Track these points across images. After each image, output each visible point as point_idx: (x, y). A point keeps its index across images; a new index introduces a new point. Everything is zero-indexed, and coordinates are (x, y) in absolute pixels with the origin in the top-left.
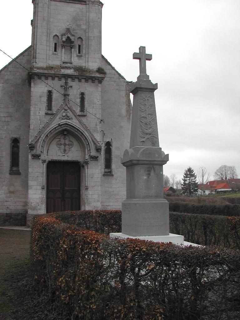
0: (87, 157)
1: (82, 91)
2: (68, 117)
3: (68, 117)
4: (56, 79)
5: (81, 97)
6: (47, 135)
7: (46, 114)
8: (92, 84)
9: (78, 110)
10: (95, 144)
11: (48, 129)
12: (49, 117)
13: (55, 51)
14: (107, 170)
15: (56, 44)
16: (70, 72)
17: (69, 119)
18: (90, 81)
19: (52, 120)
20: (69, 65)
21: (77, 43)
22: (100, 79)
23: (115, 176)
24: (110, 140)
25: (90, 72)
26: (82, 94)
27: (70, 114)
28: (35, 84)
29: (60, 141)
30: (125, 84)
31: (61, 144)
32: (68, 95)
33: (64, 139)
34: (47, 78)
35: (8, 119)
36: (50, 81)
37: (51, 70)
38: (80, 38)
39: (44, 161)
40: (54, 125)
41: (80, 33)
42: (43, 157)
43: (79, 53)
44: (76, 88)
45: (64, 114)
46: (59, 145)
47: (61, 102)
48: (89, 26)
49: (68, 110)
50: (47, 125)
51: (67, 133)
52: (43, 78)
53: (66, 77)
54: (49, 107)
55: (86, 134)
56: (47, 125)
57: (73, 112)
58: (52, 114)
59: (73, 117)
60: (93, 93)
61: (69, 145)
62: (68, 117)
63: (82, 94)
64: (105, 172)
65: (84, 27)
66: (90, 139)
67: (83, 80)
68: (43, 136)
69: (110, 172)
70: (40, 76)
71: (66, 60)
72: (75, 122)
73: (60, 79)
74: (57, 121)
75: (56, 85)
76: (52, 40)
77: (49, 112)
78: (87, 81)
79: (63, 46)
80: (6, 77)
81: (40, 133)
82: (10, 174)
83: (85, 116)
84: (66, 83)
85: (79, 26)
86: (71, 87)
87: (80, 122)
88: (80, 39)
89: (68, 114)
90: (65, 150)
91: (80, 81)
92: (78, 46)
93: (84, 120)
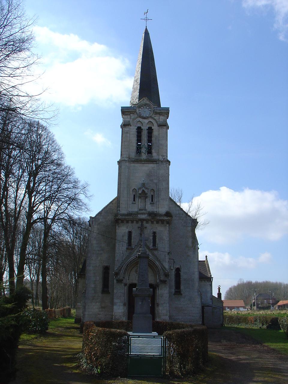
0: (158, 281)
9: (151, 246)
21: (149, 194)
28: (119, 227)
36: (130, 224)
39: (125, 285)
43: (152, 201)
53: (142, 220)
55: (157, 263)
57: (148, 248)
65: (155, 181)
68: (124, 266)
79: (140, 197)
82: (102, 293)
85: (152, 180)
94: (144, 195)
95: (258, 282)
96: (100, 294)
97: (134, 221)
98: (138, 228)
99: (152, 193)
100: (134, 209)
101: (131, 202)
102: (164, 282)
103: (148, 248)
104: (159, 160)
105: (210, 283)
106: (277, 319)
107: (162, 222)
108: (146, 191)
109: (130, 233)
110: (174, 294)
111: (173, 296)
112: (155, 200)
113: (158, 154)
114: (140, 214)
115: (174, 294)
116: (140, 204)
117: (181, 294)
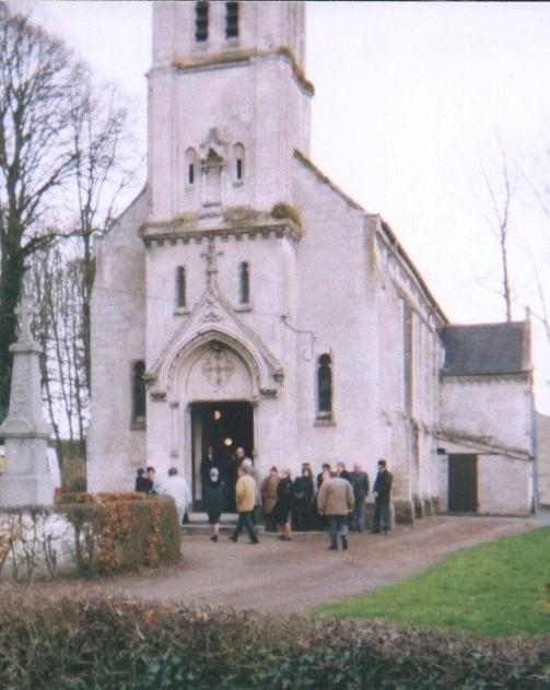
0: (256, 392)
1: (243, 260)
2: (214, 316)
3: (213, 317)
4: (180, 241)
5: (10, 343)
6: (178, 356)
7: (176, 314)
8: (265, 242)
9: (234, 299)
10: (270, 366)
11: (178, 344)
12: (182, 319)
13: (191, 181)
14: (323, 414)
15: (191, 167)
16: (214, 224)
17: (218, 320)
18: (259, 235)
19: (184, 326)
20: (214, 210)
21: (230, 157)
22: (279, 229)
23: (340, 425)
24: (328, 352)
25: (255, 217)
26: (245, 266)
27: (219, 311)
28: (152, 257)
29: (209, 363)
30: (361, 223)
31: (211, 369)
32: (215, 272)
33: (217, 358)
34: (174, 242)
35: (124, 326)
36: (180, 246)
37: (180, 225)
38: (239, 144)
39: (175, 405)
40: (190, 334)
41: (237, 135)
42: (170, 398)
43: (239, 175)
44: (232, 254)
45: (207, 312)
46: (207, 370)
47: (202, 286)
48: (255, 114)
49: (217, 304)
50: (177, 335)
51: (218, 346)
52: (167, 243)
53: (211, 234)
54: (181, 300)
55: (251, 347)
56: (177, 335)
57: (227, 306)
58: (187, 314)
59: (226, 316)
60: (271, 259)
61: (226, 369)
62: (213, 317)
63: (245, 266)
64: (319, 418)
65: (246, 118)
66: (259, 358)
67: (245, 237)
68: (170, 357)
69: (329, 418)
70: (160, 240)
71: (212, 199)
72: (228, 327)
73: (199, 241)
74: (197, 326)
75: (189, 255)
76: (182, 154)
77: (181, 310)
78: (252, 236)
79: (206, 171)
80: (118, 243)
81: (165, 351)
82: (132, 429)
83: (249, 311)
84: (211, 248)
85: (235, 118)
86: (221, 254)
87: (241, 325)
88: (239, 148)
89: (215, 311)
90: (219, 381)
91: (238, 238)
92: (236, 163)
93: (248, 319)
94: (213, 162)
95: (461, 382)
96: (128, 433)
97: (177, 238)
98: (202, 256)
99: (239, 156)
100: (190, 206)
101: (182, 187)
102: (271, 394)
103: (227, 306)
104: (256, 53)
105: (525, 387)
106: (305, 483)
107: (265, 232)
108: (219, 150)
109: (181, 271)
110: (316, 425)
111: (313, 429)
112: (247, 172)
113: (256, 35)
114: (202, 217)
115: (316, 425)
116: (205, 190)
117: (334, 425)
